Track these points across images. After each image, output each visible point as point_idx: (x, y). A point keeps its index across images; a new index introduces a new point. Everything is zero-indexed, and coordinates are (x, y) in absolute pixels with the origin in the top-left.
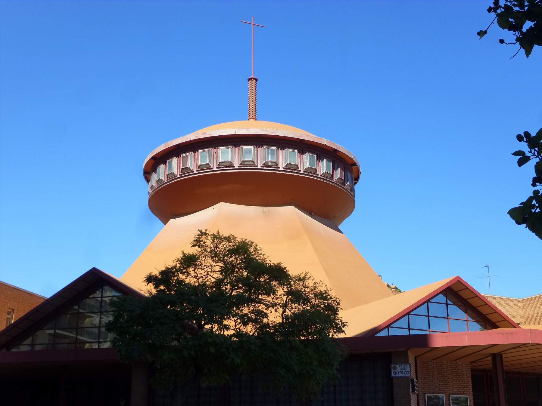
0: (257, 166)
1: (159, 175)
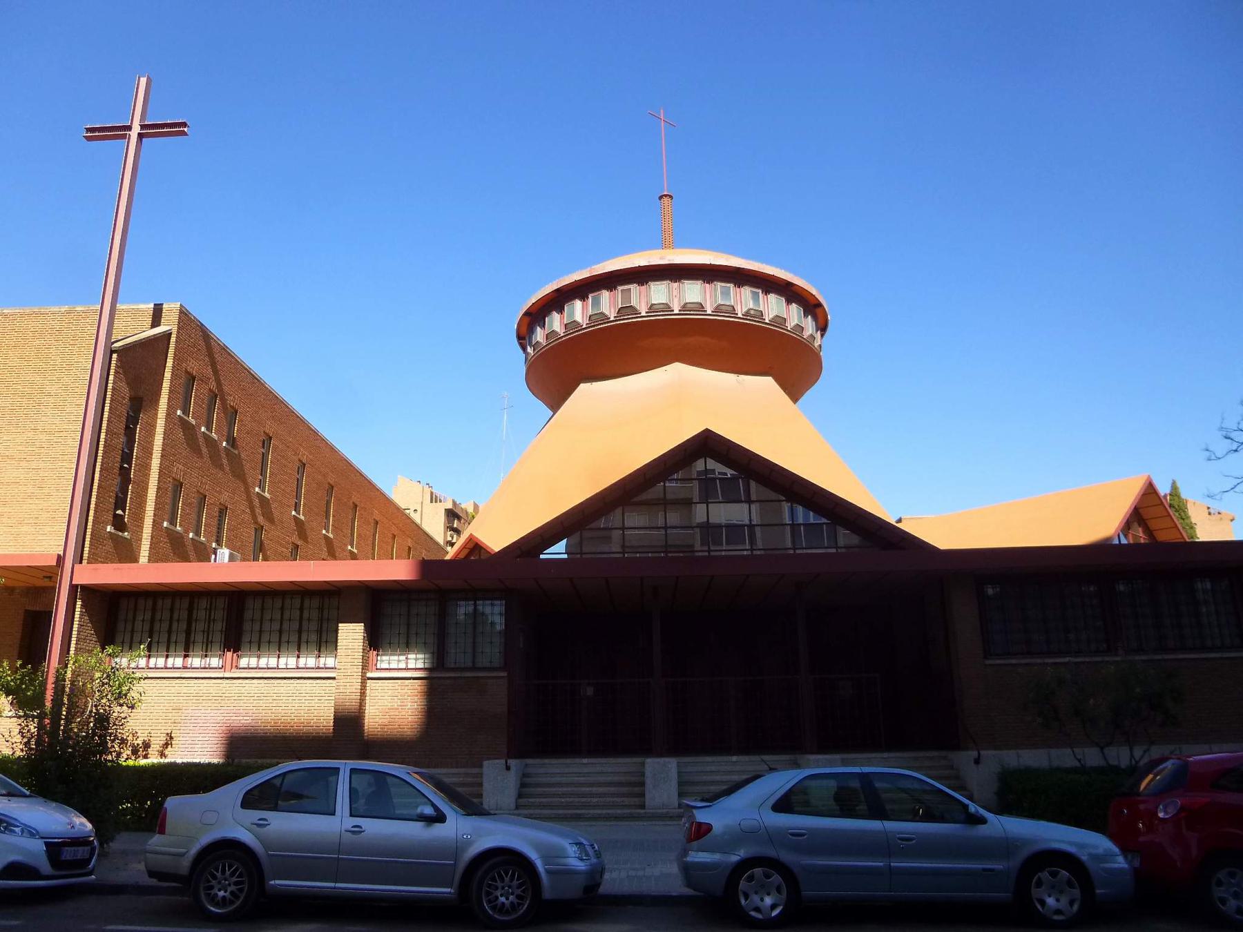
0: (673, 311)
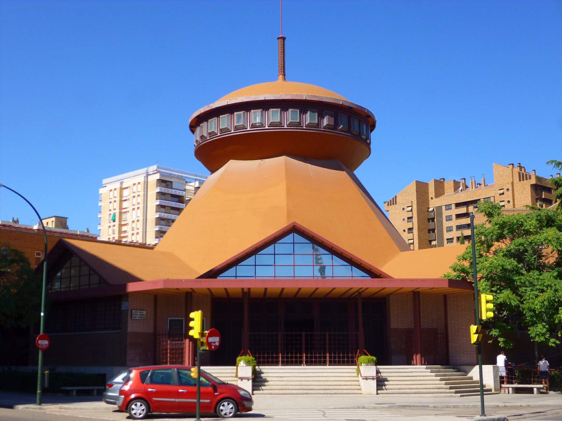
1: (196, 137)
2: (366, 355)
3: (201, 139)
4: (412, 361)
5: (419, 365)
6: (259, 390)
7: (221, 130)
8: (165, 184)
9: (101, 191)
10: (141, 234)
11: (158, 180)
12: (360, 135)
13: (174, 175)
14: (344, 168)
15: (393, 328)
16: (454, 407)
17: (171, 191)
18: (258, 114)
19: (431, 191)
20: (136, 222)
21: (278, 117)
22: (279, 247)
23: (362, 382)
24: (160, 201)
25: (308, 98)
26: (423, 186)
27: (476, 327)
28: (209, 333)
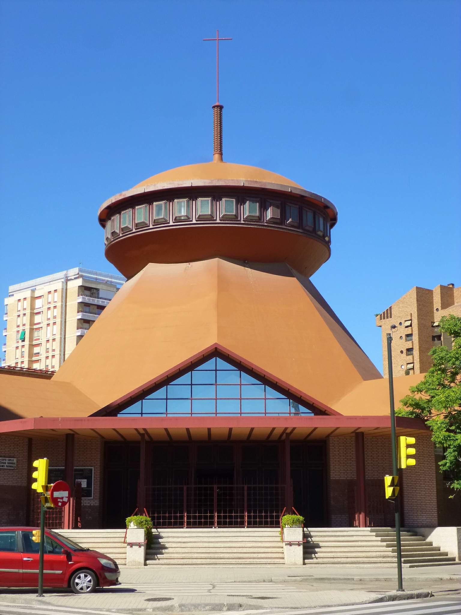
2: (294, 513)
3: (113, 236)
4: (355, 522)
5: (363, 527)
6: (155, 559)
7: (137, 225)
8: (89, 292)
9: (7, 301)
10: (57, 357)
11: (79, 287)
12: (314, 231)
13: (103, 280)
14: (294, 272)
15: (334, 479)
16: (386, 580)
17: (97, 301)
18: (183, 204)
19: (436, 300)
20: (51, 341)
21: (209, 208)
22: (197, 375)
23: (286, 548)
24: (83, 315)
25: (247, 185)
26: (426, 294)
27: (391, 477)
28: (54, 486)
